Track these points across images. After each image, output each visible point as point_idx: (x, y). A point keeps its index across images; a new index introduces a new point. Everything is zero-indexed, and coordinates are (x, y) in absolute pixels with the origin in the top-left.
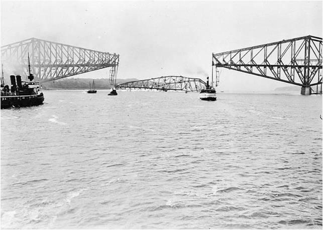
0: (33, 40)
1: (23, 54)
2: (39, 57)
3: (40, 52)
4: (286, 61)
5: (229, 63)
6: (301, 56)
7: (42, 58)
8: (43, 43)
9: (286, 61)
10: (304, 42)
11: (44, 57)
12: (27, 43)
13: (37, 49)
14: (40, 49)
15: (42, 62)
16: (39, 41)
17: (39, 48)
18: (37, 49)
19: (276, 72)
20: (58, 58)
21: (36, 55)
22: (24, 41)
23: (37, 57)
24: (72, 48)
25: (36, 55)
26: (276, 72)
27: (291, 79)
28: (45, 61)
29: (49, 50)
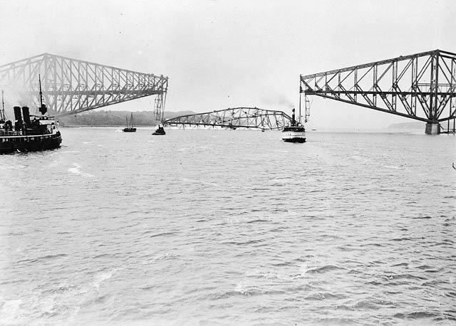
0: (46, 56)
1: (32, 77)
2: (55, 80)
3: (56, 74)
4: (405, 86)
5: (324, 90)
6: (426, 78)
7: (58, 81)
8: (60, 60)
9: (405, 86)
10: (430, 59)
11: (62, 81)
12: (38, 61)
13: (52, 68)
14: (55, 70)
15: (58, 87)
16: (54, 57)
17: (55, 67)
18: (52, 68)
19: (391, 103)
20: (82, 82)
21: (51, 77)
22: (32, 58)
23: (51, 81)
24: (101, 67)
25: (51, 77)
26: (391, 103)
27: (412, 111)
28: (63, 86)
29: (69, 71)
